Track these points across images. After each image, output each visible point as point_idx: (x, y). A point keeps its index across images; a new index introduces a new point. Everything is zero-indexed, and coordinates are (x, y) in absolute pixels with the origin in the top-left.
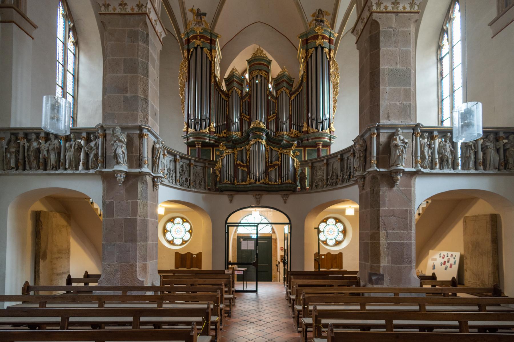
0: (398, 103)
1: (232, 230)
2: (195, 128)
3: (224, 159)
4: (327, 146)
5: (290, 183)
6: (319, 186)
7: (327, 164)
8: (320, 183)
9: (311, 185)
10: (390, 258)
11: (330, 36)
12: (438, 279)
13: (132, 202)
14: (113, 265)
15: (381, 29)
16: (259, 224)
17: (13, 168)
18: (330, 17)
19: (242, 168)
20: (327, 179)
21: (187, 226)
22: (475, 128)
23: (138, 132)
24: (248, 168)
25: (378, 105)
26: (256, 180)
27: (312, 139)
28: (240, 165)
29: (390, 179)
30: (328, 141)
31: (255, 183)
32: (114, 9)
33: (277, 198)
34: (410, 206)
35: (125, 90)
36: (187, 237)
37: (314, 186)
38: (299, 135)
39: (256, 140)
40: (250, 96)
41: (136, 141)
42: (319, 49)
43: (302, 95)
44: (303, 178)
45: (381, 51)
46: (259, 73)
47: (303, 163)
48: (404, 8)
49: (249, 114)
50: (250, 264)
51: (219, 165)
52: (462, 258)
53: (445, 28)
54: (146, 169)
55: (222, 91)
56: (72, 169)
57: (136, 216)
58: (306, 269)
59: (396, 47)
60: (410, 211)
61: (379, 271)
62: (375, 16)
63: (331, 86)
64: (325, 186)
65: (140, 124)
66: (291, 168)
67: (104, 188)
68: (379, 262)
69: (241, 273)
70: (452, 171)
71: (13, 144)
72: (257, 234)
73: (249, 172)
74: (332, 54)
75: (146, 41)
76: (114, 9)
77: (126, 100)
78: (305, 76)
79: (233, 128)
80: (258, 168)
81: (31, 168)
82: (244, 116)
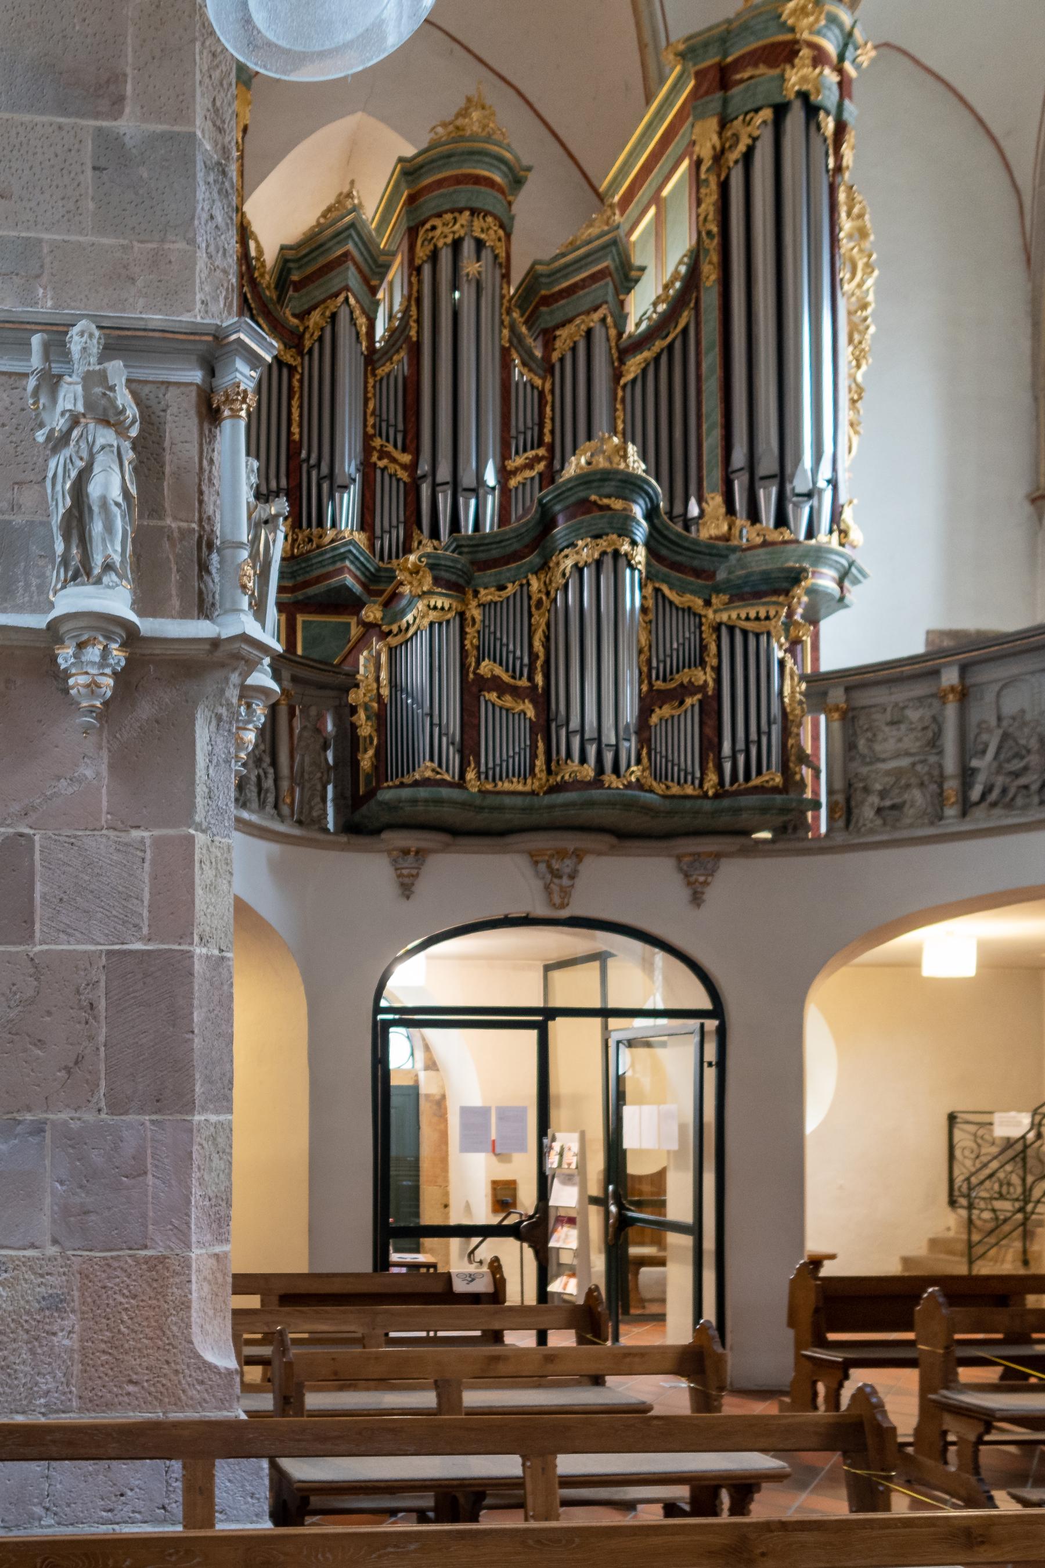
9: (845, 810)
13: (158, 843)
14: (26, 1262)
19: (508, 701)
20: (967, 775)
23: (197, 376)
24: (543, 700)
26: (600, 769)
28: (501, 688)
31: (597, 782)
35: (105, 92)
40: (415, 350)
42: (796, 118)
57: (185, 934)
64: (951, 812)
73: (545, 725)
77: (112, 155)
80: (607, 699)
82: (383, 454)
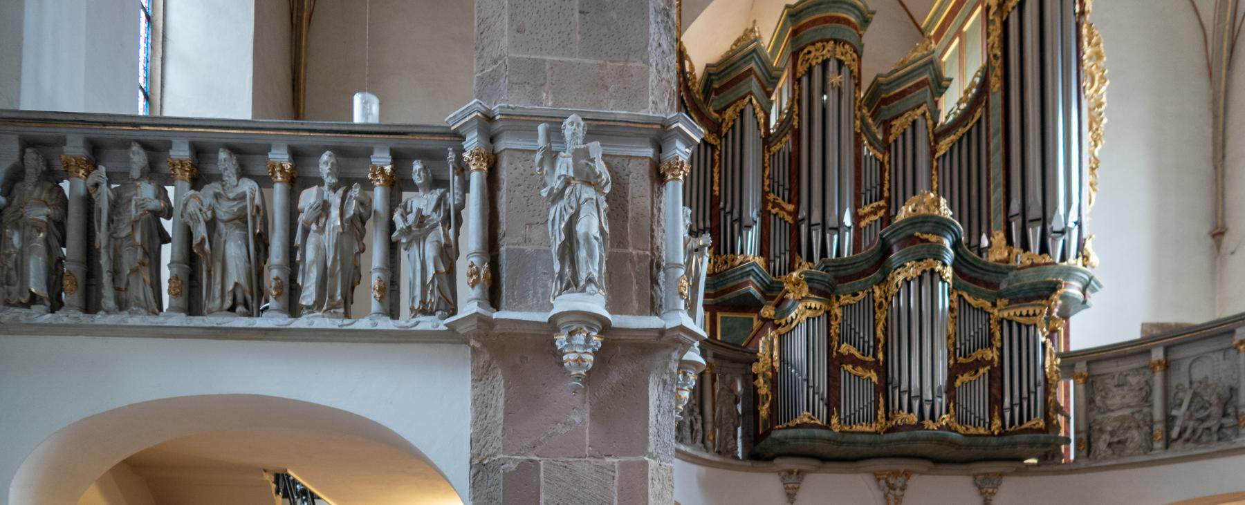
6: (1130, 445)
9: (1086, 445)
13: (623, 466)
17: (34, 299)
19: (860, 371)
23: (649, 152)
24: (883, 370)
26: (921, 416)
31: (920, 425)
40: (797, 134)
49: (794, 197)
64: (1158, 445)
67: (481, 407)
71: (31, 189)
80: (927, 370)
81: (122, 305)
82: (775, 205)
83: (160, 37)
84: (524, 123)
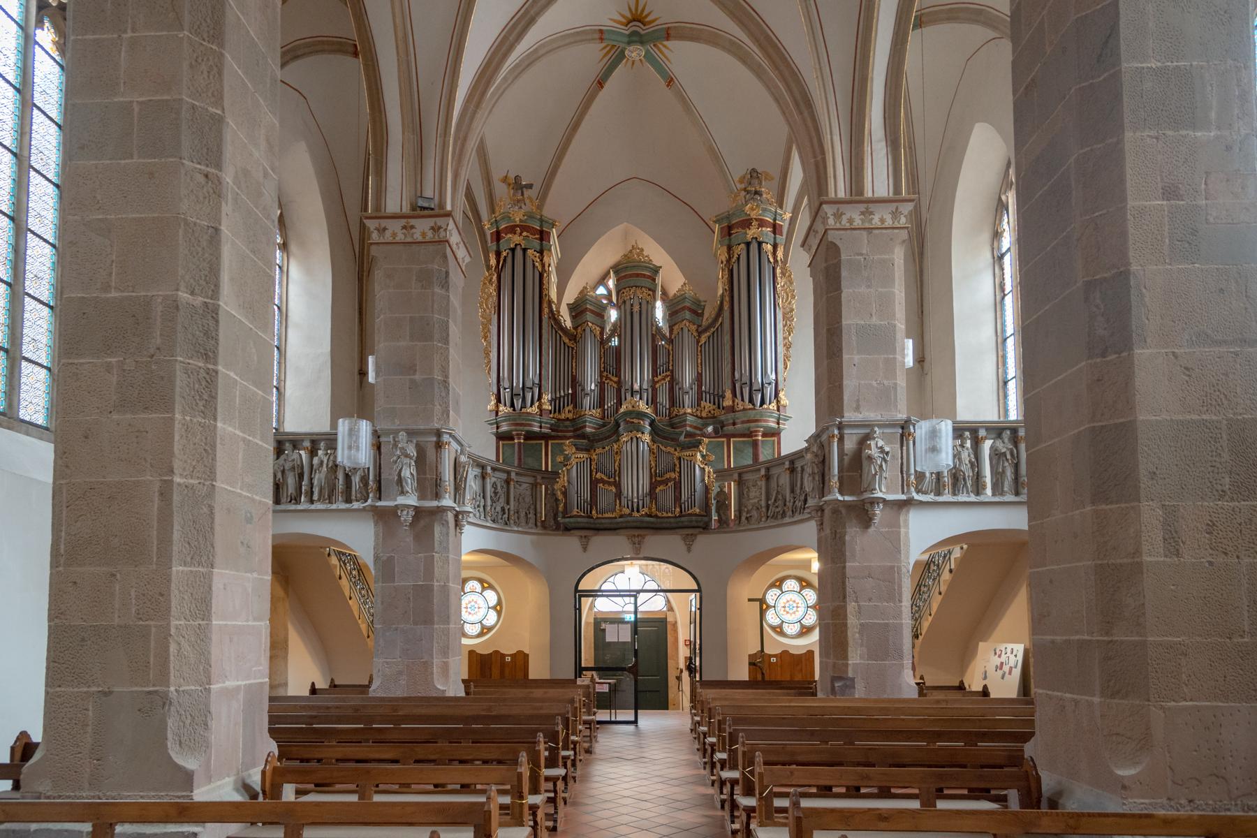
0: (874, 383)
1: (586, 602)
2: (512, 405)
3: (574, 467)
4: (773, 435)
5: (696, 515)
7: (768, 477)
8: (754, 513)
10: (865, 650)
11: (775, 220)
12: (992, 696)
15: (843, 257)
16: (639, 592)
18: (775, 183)
19: (607, 487)
20: (768, 507)
21: (491, 597)
22: (943, 455)
24: (618, 485)
25: (841, 387)
27: (743, 422)
28: (602, 481)
29: (862, 513)
30: (775, 426)
31: (630, 515)
32: (394, 235)
33: (672, 542)
34: (899, 560)
35: (412, 369)
36: (492, 619)
37: (743, 518)
38: (717, 412)
39: (631, 435)
41: (431, 452)
42: (754, 246)
43: (722, 326)
44: (723, 506)
45: (843, 295)
46: (634, 294)
47: (722, 474)
48: (882, 220)
50: (623, 669)
51: (562, 481)
52: (1026, 652)
53: (1003, 198)
54: (447, 501)
55: (564, 330)
56: (323, 502)
57: (432, 580)
58: (731, 677)
59: (869, 287)
60: (899, 568)
61: (847, 672)
62: (832, 236)
63: (780, 316)
65: (437, 426)
66: (699, 486)
67: (376, 535)
68: (846, 658)
69: (605, 689)
70: (973, 498)
72: (636, 612)
73: (619, 495)
74: (780, 254)
75: (445, 284)
76: (394, 235)
78: (727, 299)
79: (587, 402)
80: (635, 483)
83: (285, 317)
84: (388, 433)
